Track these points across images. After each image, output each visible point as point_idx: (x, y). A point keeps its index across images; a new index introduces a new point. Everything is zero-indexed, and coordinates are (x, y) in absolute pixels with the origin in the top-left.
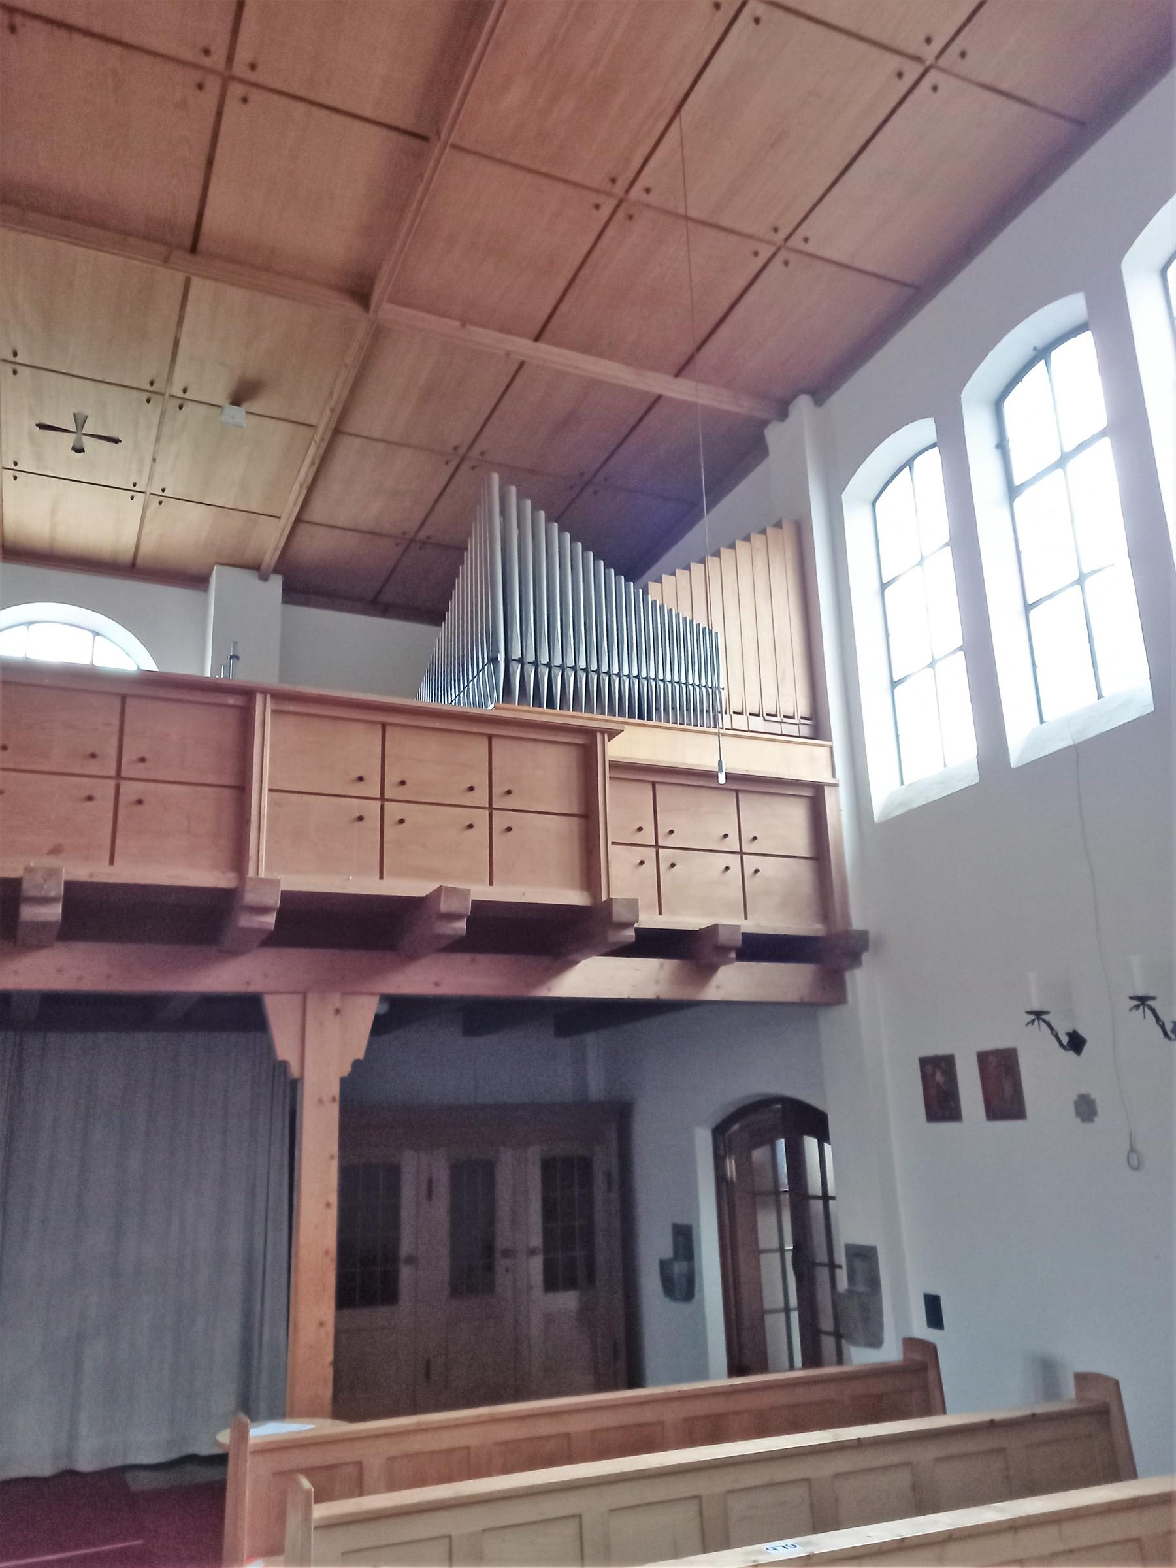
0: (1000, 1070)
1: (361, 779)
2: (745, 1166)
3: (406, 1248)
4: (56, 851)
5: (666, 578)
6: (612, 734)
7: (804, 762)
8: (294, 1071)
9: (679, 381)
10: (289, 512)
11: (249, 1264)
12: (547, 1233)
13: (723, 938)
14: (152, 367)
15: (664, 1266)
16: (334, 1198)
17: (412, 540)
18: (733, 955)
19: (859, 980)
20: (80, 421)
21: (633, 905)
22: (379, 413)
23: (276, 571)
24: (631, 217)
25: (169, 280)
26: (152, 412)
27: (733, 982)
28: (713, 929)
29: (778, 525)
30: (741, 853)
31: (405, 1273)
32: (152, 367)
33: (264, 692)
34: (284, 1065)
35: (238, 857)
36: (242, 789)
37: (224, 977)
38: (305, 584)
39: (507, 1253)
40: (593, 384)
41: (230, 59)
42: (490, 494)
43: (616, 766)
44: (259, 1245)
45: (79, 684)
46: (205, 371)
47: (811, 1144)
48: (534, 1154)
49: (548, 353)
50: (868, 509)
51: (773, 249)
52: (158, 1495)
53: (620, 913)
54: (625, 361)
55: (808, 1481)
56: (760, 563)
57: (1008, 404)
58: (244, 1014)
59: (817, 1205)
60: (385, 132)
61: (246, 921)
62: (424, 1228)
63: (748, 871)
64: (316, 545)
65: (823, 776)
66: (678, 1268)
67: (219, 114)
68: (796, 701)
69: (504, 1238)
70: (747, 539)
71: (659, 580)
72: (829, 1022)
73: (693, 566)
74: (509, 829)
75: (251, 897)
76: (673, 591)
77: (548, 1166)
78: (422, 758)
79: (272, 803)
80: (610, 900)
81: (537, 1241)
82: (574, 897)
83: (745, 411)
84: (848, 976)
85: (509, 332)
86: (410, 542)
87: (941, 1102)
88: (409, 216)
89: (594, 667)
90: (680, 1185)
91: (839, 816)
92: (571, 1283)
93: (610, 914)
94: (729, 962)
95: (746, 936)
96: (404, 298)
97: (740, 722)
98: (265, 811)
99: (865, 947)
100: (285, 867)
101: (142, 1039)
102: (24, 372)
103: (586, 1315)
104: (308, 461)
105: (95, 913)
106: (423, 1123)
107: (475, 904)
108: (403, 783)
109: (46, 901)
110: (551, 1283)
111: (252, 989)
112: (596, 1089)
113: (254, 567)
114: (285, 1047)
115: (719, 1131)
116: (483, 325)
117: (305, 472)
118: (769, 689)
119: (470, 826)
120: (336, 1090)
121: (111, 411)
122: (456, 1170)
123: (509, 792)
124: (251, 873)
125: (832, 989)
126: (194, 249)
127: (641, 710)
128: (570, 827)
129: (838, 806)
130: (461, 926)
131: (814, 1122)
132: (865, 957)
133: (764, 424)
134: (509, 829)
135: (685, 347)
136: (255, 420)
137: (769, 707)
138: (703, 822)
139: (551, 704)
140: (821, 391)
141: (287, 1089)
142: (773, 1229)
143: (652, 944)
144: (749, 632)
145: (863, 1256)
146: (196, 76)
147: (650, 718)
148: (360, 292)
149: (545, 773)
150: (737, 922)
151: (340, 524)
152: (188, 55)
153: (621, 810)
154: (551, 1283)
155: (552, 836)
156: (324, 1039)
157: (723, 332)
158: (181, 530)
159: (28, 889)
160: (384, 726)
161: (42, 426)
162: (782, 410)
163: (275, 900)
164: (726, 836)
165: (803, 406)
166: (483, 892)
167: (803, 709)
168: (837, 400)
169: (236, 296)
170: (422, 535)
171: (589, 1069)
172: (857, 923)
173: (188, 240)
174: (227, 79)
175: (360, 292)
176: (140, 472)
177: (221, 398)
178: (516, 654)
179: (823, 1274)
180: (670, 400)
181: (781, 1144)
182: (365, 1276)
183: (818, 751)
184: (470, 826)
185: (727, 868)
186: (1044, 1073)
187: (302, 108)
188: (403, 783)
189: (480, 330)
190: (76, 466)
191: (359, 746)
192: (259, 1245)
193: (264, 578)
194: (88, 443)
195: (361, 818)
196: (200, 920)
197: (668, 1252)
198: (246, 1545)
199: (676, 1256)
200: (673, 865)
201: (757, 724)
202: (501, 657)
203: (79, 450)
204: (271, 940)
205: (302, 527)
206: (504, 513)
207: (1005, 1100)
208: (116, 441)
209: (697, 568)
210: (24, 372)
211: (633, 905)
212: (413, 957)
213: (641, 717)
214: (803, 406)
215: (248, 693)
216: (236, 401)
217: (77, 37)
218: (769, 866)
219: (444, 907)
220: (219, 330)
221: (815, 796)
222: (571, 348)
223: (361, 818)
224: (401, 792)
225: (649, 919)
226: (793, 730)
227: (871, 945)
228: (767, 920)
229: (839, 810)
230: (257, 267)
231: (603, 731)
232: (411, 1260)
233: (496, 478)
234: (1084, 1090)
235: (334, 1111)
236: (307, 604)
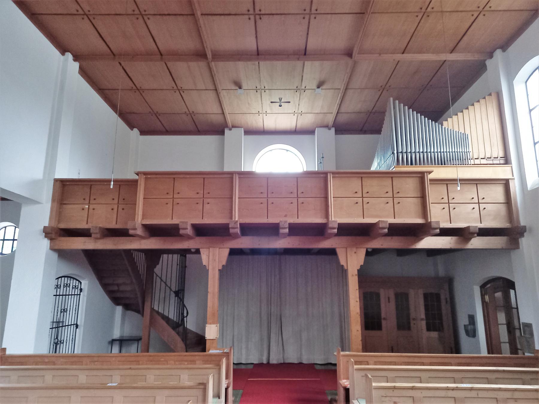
1: (356, 192)
2: (492, 298)
3: (383, 315)
4: (286, 216)
5: (449, 119)
6: (430, 172)
7: (502, 173)
8: (345, 267)
9: (452, 54)
10: (335, 111)
11: (340, 316)
12: (427, 315)
13: (472, 230)
14: (296, 83)
16: (358, 300)
17: (371, 113)
18: (476, 235)
19: (524, 242)
20: (280, 99)
21: (438, 223)
22: (359, 81)
23: (333, 127)
24: (428, 16)
25: (299, 64)
26: (298, 94)
27: (476, 243)
28: (468, 228)
29: (490, 95)
30: (479, 203)
31: (384, 323)
32: (296, 83)
33: (330, 173)
34: (343, 266)
35: (327, 216)
36: (326, 198)
37: (326, 244)
38: (341, 129)
39: (414, 319)
40: (422, 62)
41: (311, 10)
42: (390, 104)
43: (431, 180)
44: (343, 311)
45: (110, 185)
46: (310, 82)
48: (421, 292)
49: (407, 57)
50: (524, 84)
51: (479, 13)
52: (319, 371)
53: (434, 225)
54: (433, 53)
55: (487, 378)
56: (483, 109)
58: (332, 252)
59: (515, 311)
60: (352, 15)
61: (330, 231)
62: (388, 310)
63: (481, 209)
64: (343, 118)
65: (509, 176)
66: (470, 327)
67: (309, 22)
69: (413, 315)
70: (478, 101)
71: (447, 120)
72: (514, 255)
73: (459, 114)
74: (399, 203)
75: (330, 225)
76: (452, 123)
77: (426, 296)
78: (372, 185)
79: (334, 201)
80: (431, 222)
81: (423, 316)
82: (420, 221)
83: (477, 59)
84: (520, 240)
85: (394, 53)
86: (370, 113)
88: (361, 33)
89: (425, 151)
90: (471, 304)
91: (515, 189)
92: (435, 330)
93: (431, 226)
94: (476, 237)
95: (480, 229)
96: (361, 52)
98: (332, 203)
99: (525, 231)
100: (339, 217)
101: (308, 257)
102: (267, 91)
103: (440, 338)
104: (339, 98)
106: (386, 281)
107: (389, 224)
108: (368, 192)
109: (285, 228)
110: (428, 329)
111: (333, 247)
112: (442, 273)
113: (327, 127)
114: (342, 262)
116: (386, 54)
117: (338, 101)
119: (387, 203)
121: (287, 96)
122: (397, 295)
123: (398, 192)
124: (330, 219)
126: (305, 54)
127: (442, 163)
128: (417, 201)
129: (515, 187)
130: (386, 230)
131: (511, 285)
132: (525, 234)
133: (485, 60)
134: (399, 203)
135: (452, 45)
136: (324, 91)
137: (488, 155)
138: (460, 194)
139: (412, 164)
140: (504, 47)
141: (343, 272)
142: (502, 318)
143: (445, 232)
145: (528, 326)
146: (303, 16)
147: (445, 164)
148: (349, 54)
149: (410, 186)
150: (477, 225)
151: (349, 111)
152: (300, 12)
153: (433, 194)
154: (428, 329)
156: (353, 260)
157: (465, 38)
158: (307, 121)
159: (281, 225)
160: (362, 178)
161: (272, 102)
162: (491, 55)
163: (336, 226)
164: (473, 198)
165: (498, 53)
166: (392, 221)
167: (501, 154)
168: (512, 49)
169: (317, 63)
170: (374, 111)
171: (428, 269)
173: (303, 53)
174: (310, 14)
175: (349, 54)
176: (296, 108)
177: (315, 87)
178: (400, 150)
180: (449, 61)
182: (371, 322)
183: (507, 168)
184: (387, 203)
185: (474, 208)
187: (330, 15)
188: (368, 192)
189: (386, 55)
190: (280, 110)
191: (355, 184)
192: (343, 311)
193: (330, 129)
194: (282, 104)
195: (357, 203)
196: (320, 230)
197: (467, 323)
198: (342, 377)
199: (470, 324)
200: (454, 208)
202: (395, 152)
203: (280, 106)
204: (337, 235)
205: (339, 114)
206: (394, 108)
208: (289, 102)
209: (460, 114)
210: (267, 91)
211: (438, 223)
212: (375, 238)
213: (442, 164)
214: (498, 53)
215: (326, 174)
216: (318, 87)
217: (275, 16)
218: (489, 207)
219: (380, 226)
220: (312, 70)
221: (506, 183)
222: (414, 53)
223: (357, 203)
224: (367, 195)
226: (498, 162)
227: (527, 230)
229: (515, 187)
230: (321, 55)
231: (427, 172)
232: (384, 319)
233: (392, 99)
235: (357, 278)
236: (342, 134)
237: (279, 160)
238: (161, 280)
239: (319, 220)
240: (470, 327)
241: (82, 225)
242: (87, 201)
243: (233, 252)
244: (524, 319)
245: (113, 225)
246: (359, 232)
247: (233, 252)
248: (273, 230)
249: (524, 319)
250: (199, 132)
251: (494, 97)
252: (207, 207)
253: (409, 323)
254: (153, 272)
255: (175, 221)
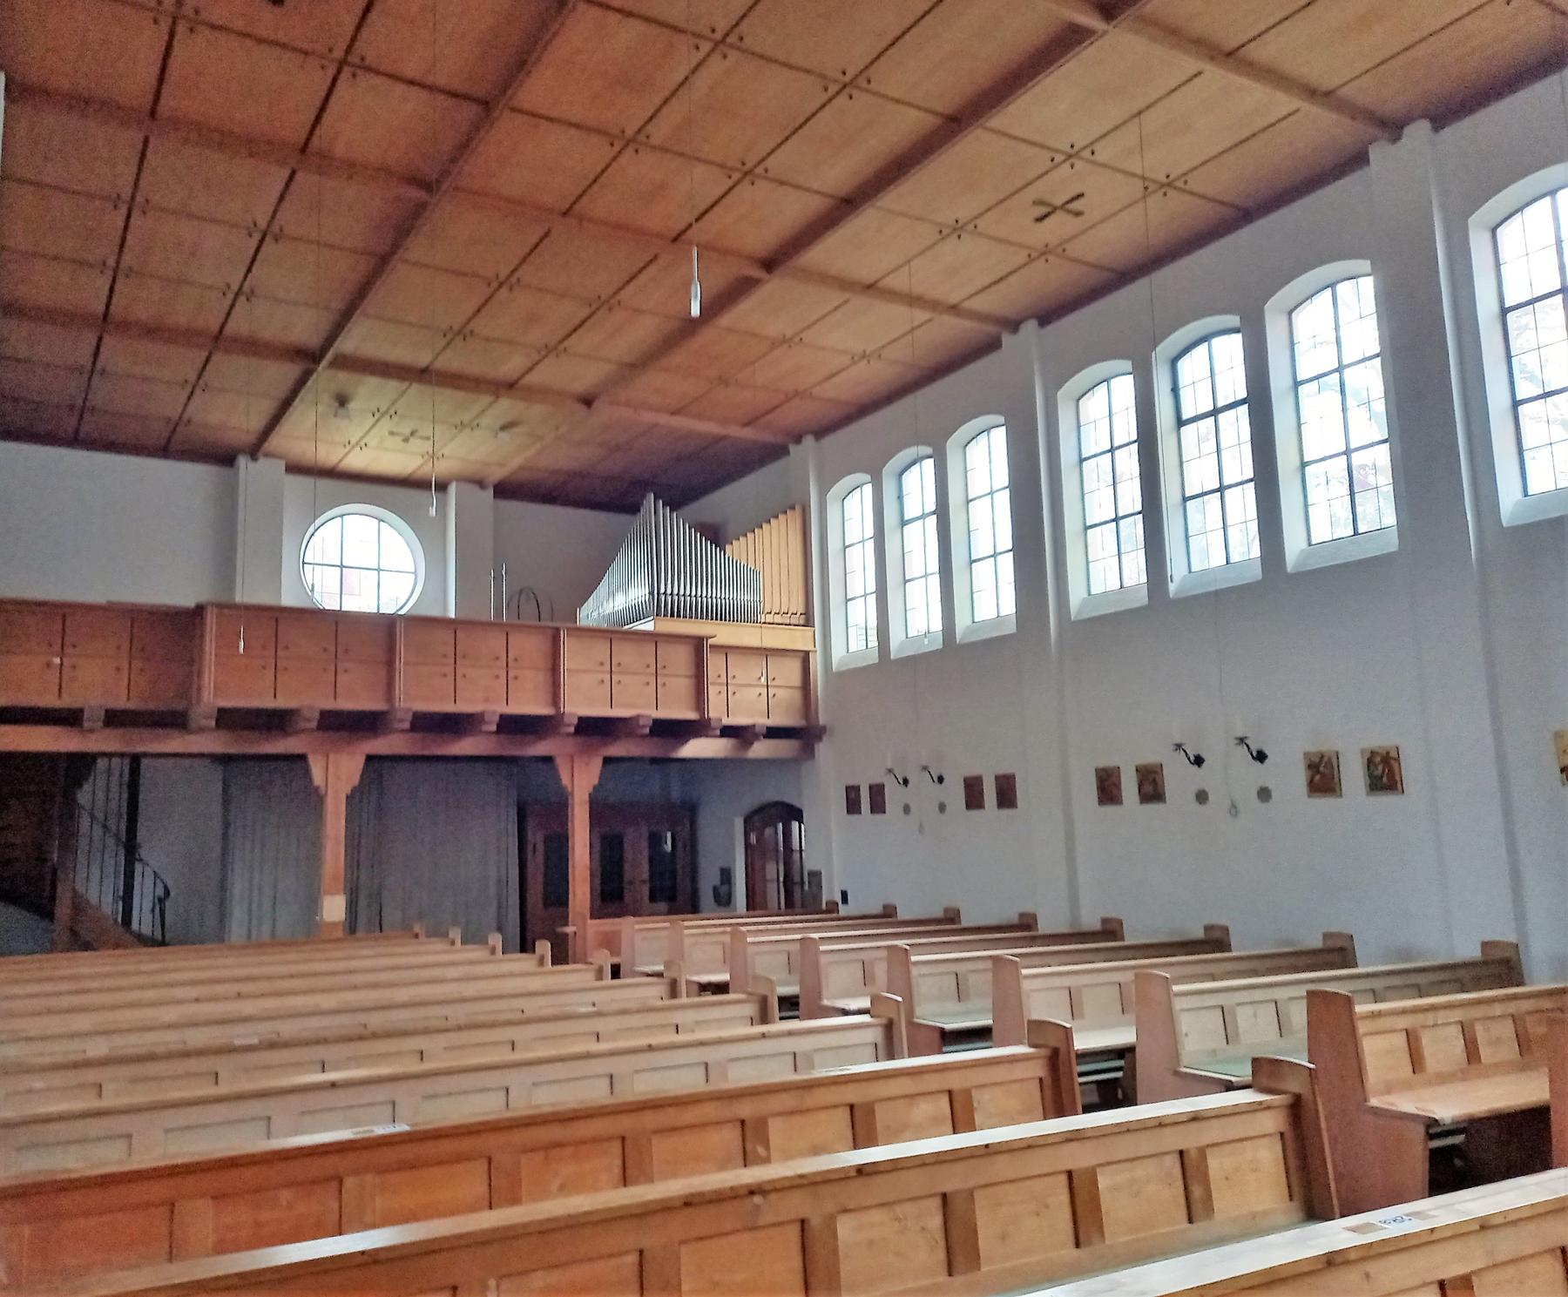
0: (877, 792)
7: (798, 639)
13: (757, 730)
15: (715, 889)
19: (822, 749)
29: (793, 508)
35: (555, 699)
37: (541, 748)
38: (504, 490)
39: (631, 883)
47: (795, 825)
53: (713, 724)
57: (1180, 364)
58: (302, 758)
66: (724, 889)
68: (798, 605)
76: (737, 549)
78: (626, 654)
81: (646, 876)
82: (692, 715)
87: (853, 806)
97: (769, 618)
100: (581, 702)
105: (514, 726)
114: (565, 781)
115: (747, 820)
118: (785, 599)
120: (587, 797)
125: (808, 751)
129: (816, 663)
131: (796, 814)
138: (747, 672)
140: (821, 432)
141: (314, 800)
144: (775, 569)
145: (815, 875)
149: (680, 657)
150: (762, 721)
155: (681, 685)
156: (581, 780)
159: (487, 718)
162: (798, 439)
165: (809, 441)
167: (801, 610)
168: (829, 441)
172: (822, 721)
179: (797, 889)
181: (780, 826)
186: (1178, 777)
197: (717, 881)
199: (722, 883)
201: (778, 619)
207: (878, 806)
209: (750, 535)
214: (809, 441)
218: (781, 693)
221: (805, 657)
225: (726, 721)
226: (795, 620)
228: (778, 720)
234: (1265, 805)
237: (363, 563)
238: (93, 817)
239: (543, 710)
240: (724, 889)
241: (49, 701)
242: (57, 648)
243: (370, 759)
244: (809, 865)
245: (121, 703)
246: (595, 729)
247: (370, 759)
248: (455, 724)
249: (809, 865)
250: (165, 450)
251: (794, 518)
252: (342, 677)
253: (621, 890)
254: (74, 800)
255: (281, 703)
